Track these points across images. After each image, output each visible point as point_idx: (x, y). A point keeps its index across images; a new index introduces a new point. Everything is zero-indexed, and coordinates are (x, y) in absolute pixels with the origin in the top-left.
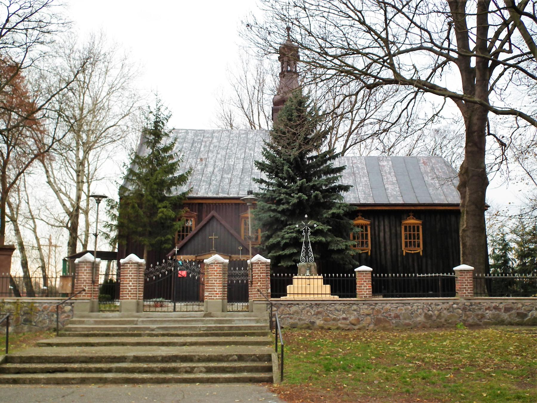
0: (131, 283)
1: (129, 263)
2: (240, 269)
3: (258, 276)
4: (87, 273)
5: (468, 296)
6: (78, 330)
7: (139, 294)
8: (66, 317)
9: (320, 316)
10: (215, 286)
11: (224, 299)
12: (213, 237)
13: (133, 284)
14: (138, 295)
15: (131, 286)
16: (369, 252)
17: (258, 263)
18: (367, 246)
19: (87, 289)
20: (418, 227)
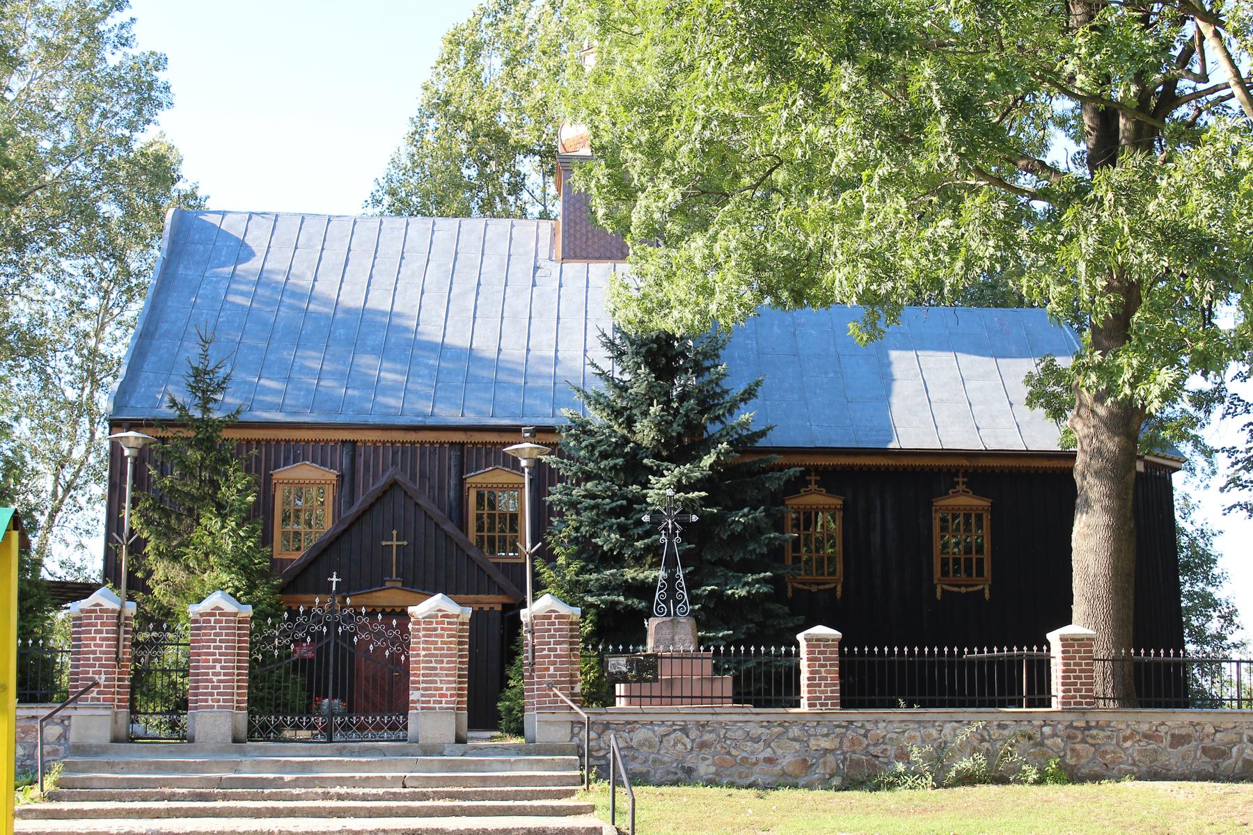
0: (218, 665)
1: (213, 615)
3: (550, 650)
4: (103, 639)
5: (1081, 703)
7: (239, 694)
10: (436, 675)
11: (461, 709)
12: (395, 543)
13: (222, 668)
14: (235, 698)
15: (218, 674)
16: (839, 588)
17: (550, 617)
18: (833, 573)
19: (102, 679)
20: (979, 518)
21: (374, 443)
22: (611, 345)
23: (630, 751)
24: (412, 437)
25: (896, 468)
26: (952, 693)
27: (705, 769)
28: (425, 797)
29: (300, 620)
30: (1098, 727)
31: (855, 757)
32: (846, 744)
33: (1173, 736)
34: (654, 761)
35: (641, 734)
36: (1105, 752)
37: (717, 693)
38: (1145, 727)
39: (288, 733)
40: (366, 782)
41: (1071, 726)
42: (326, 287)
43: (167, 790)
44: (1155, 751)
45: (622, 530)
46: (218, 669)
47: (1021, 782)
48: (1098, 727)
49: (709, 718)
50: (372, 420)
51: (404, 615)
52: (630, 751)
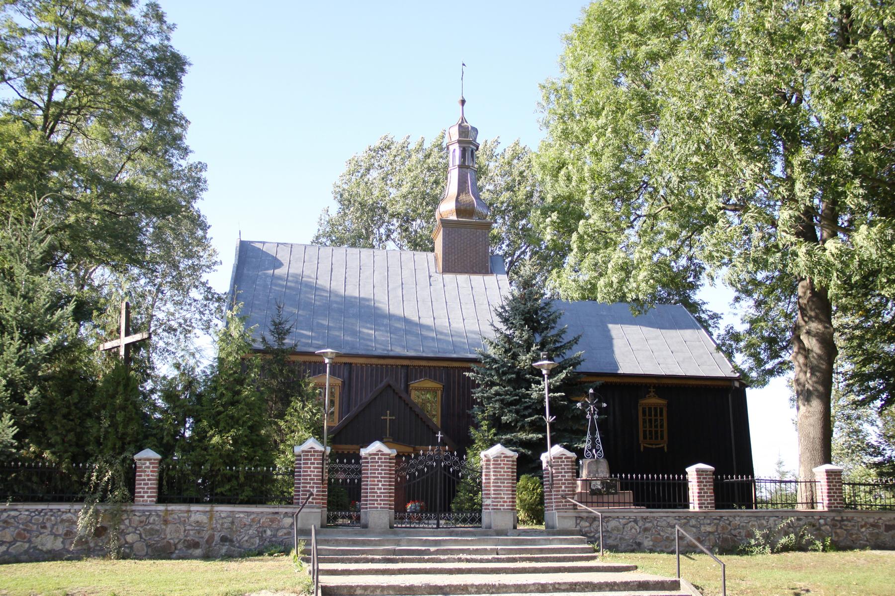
1: (377, 455)
2: (349, 462)
4: (315, 468)
6: (324, 552)
8: (285, 534)
9: (647, 534)
12: (388, 418)
21: (361, 364)
22: (500, 315)
23: (607, 533)
24: (381, 362)
25: (620, 383)
26: (659, 501)
27: (647, 543)
28: (514, 560)
29: (420, 458)
30: (848, 520)
31: (725, 536)
32: (720, 529)
33: (886, 525)
34: (621, 539)
35: (613, 524)
36: (852, 534)
37: (627, 500)
38: (871, 520)
39: (340, 521)
40: (476, 552)
41: (833, 519)
42: (323, 282)
43: (370, 557)
44: (878, 534)
45: (517, 412)
46: (380, 486)
47: (815, 550)
48: (848, 520)
49: (648, 514)
50: (360, 352)
51: (358, 457)
52: (607, 533)
